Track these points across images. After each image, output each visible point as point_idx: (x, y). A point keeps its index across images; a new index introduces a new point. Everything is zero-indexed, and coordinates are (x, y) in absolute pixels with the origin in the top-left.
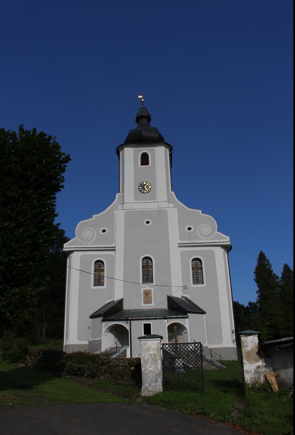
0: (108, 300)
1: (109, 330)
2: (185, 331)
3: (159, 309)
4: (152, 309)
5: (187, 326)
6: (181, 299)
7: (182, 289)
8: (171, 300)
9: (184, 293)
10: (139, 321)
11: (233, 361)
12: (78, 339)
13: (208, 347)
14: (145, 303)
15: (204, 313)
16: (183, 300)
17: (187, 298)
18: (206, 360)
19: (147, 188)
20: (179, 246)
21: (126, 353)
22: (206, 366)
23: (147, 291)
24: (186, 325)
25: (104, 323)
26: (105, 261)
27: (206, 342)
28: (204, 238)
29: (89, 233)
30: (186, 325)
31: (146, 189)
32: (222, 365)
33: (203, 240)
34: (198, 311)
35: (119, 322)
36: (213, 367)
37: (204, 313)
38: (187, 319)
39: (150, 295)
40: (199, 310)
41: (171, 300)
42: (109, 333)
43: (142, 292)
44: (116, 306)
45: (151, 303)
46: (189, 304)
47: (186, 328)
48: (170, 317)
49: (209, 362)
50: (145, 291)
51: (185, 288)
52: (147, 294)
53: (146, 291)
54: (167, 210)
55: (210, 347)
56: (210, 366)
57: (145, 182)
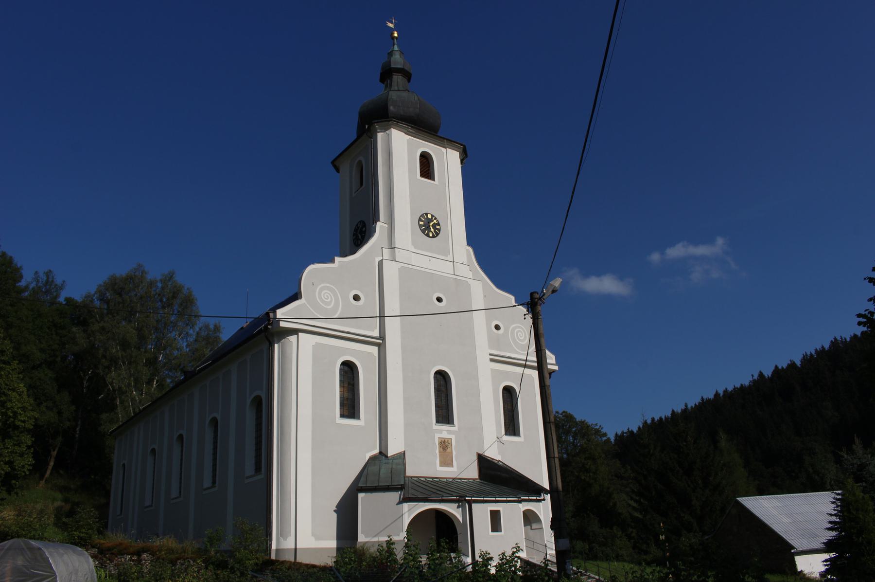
8: (483, 462)
10: (482, 504)
12: (313, 535)
19: (433, 228)
20: (492, 360)
25: (406, 506)
26: (360, 364)
28: (519, 351)
29: (327, 296)
31: (432, 230)
33: (517, 353)
35: (442, 504)
39: (449, 450)
41: (483, 462)
48: (497, 499)
52: (445, 445)
53: (443, 440)
54: (469, 283)
57: (430, 215)
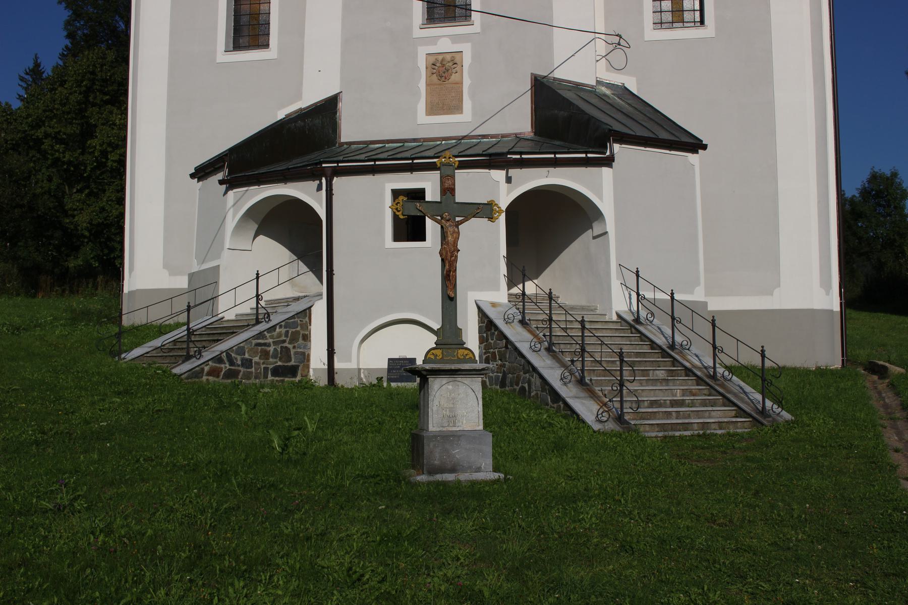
0: (283, 106)
1: (254, 227)
2: (597, 229)
3: (493, 136)
4: (464, 138)
5: (605, 204)
6: (592, 91)
7: (601, 47)
9: (611, 66)
11: (821, 372)
12: (166, 266)
13: (705, 304)
14: (433, 109)
15: (695, 145)
16: (605, 95)
17: (624, 91)
18: (688, 372)
21: (307, 326)
22: (681, 403)
23: (443, 60)
24: (601, 198)
27: (698, 284)
30: (601, 198)
32: (768, 404)
34: (664, 135)
35: (290, 184)
36: (719, 415)
37: (695, 145)
38: (605, 170)
39: (454, 77)
40: (672, 133)
42: (262, 238)
43: (422, 64)
44: (300, 123)
45: (456, 107)
46: (630, 109)
47: (597, 214)
49: (699, 380)
50: (432, 59)
51: (618, 42)
53: (440, 58)
55: (716, 304)
56: (704, 403)
